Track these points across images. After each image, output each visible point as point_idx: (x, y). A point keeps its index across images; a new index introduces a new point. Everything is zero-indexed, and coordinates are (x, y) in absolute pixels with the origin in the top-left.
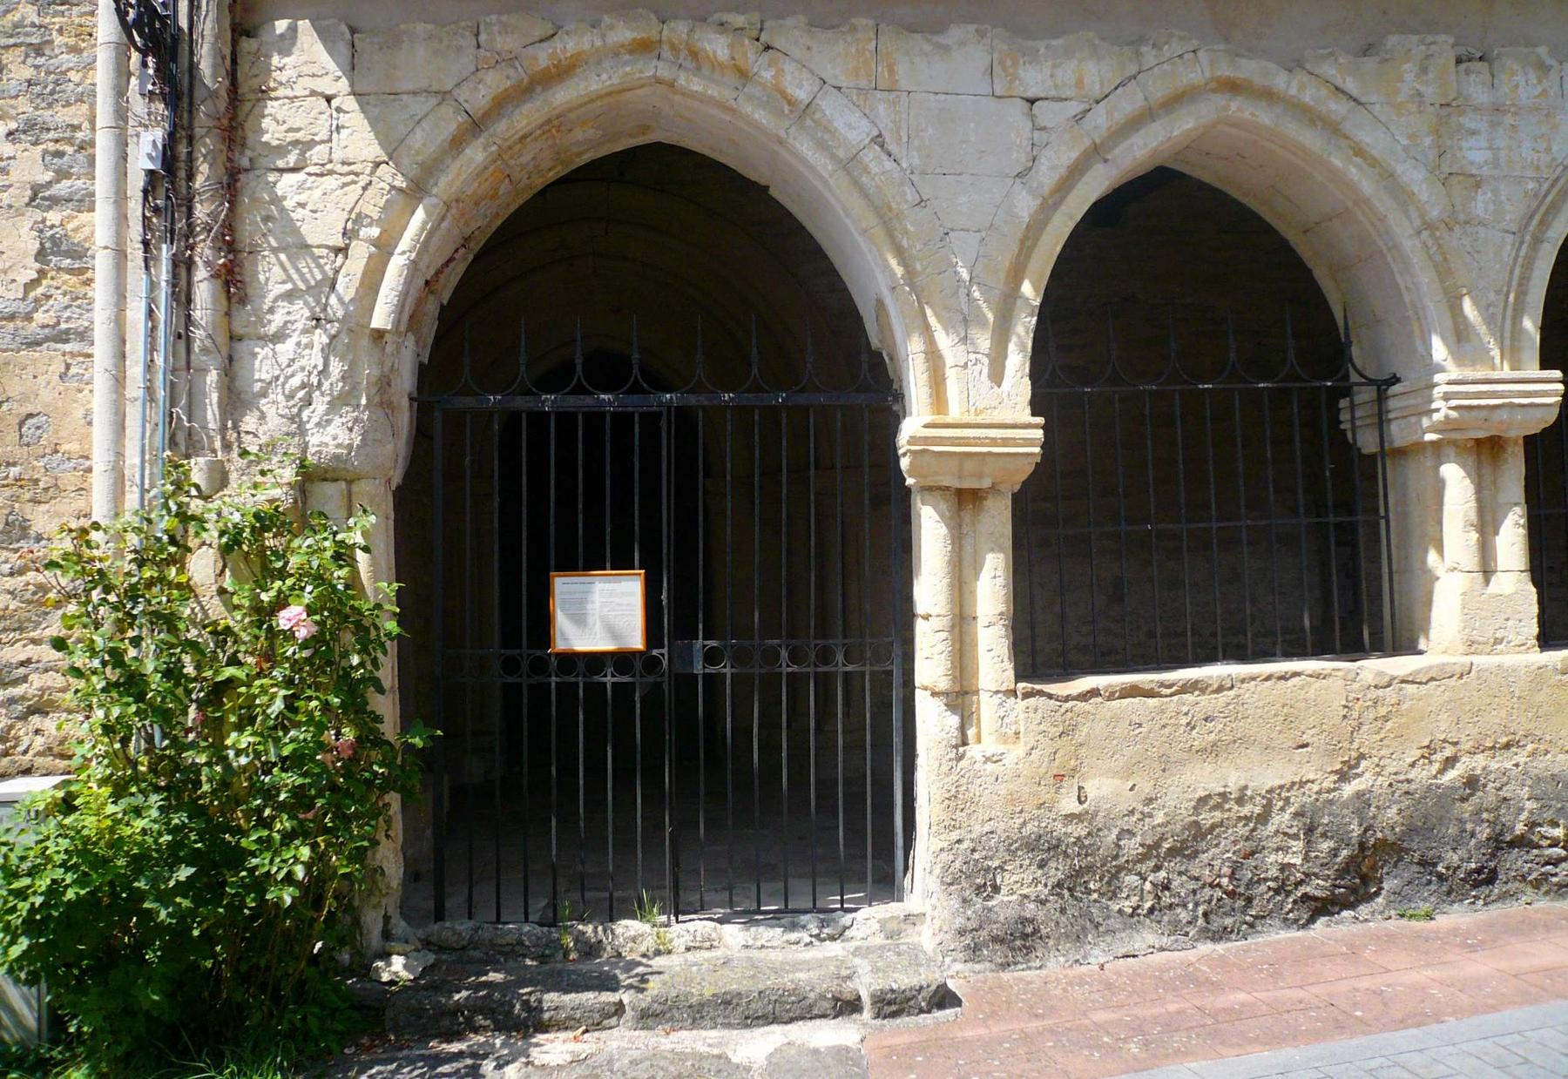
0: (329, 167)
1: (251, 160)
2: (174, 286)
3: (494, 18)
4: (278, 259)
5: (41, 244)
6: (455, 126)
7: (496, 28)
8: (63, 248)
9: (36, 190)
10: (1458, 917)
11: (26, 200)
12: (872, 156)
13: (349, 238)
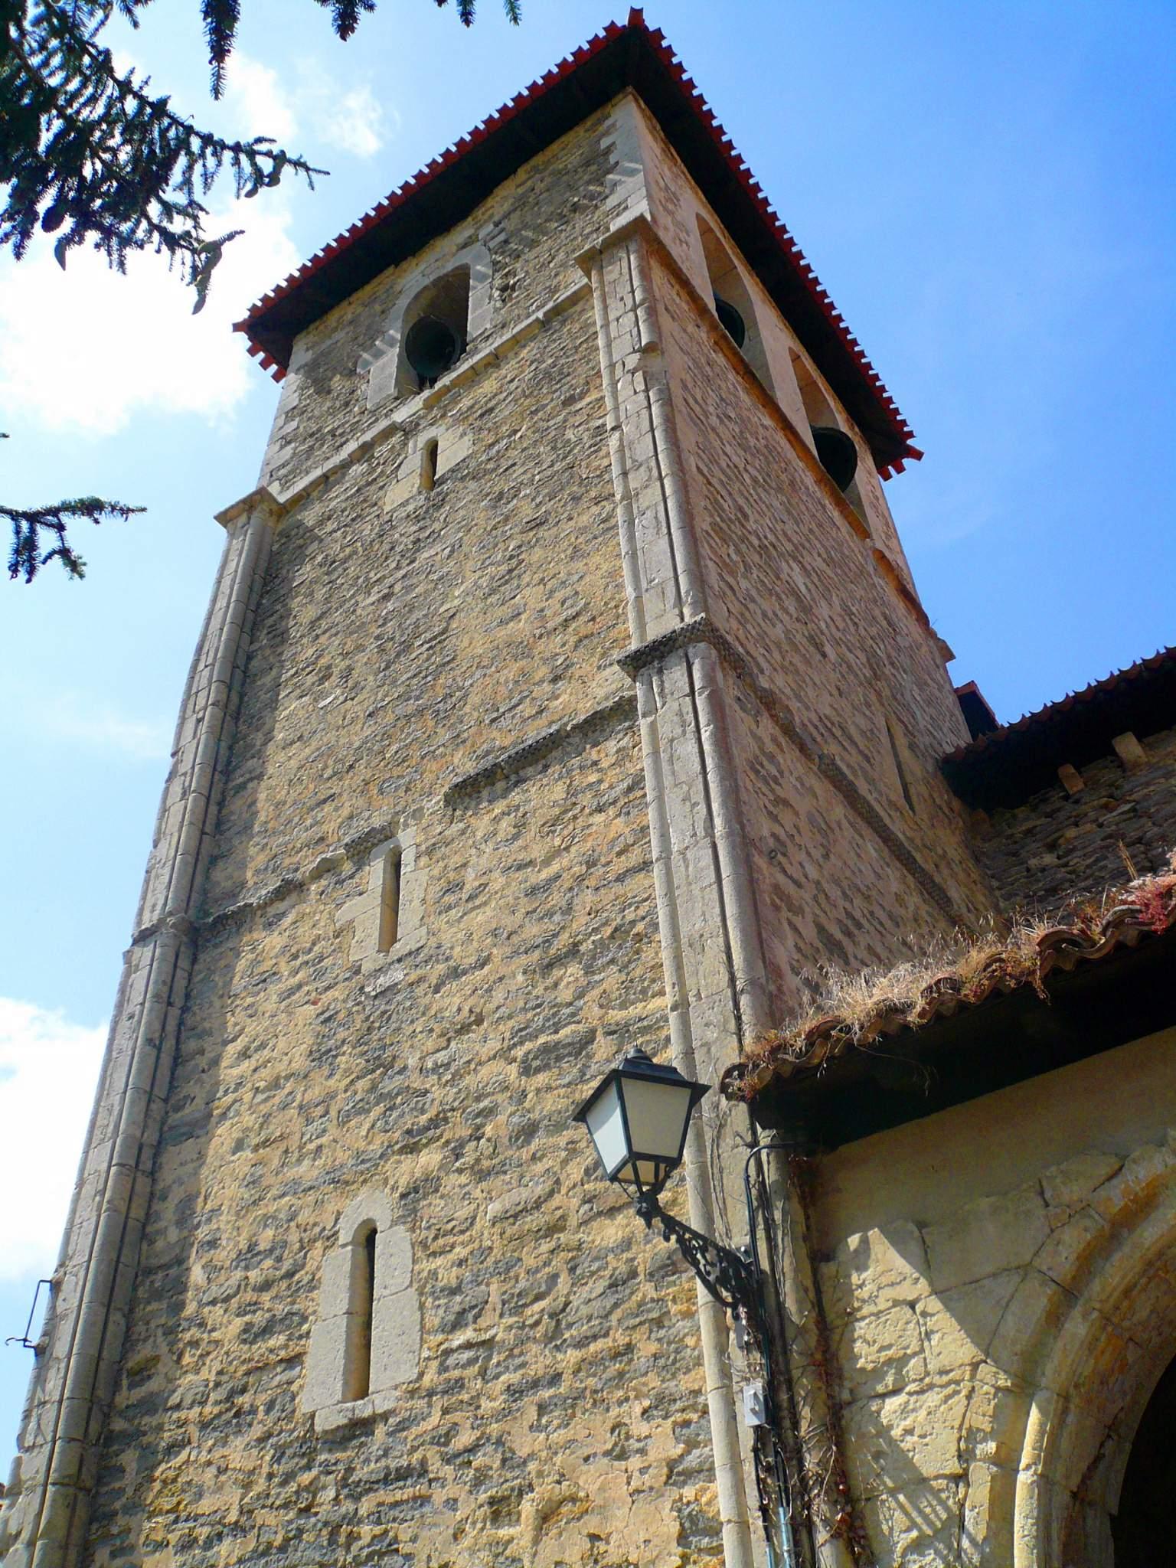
0: (927, 1380)
1: (851, 1391)
2: (797, 1555)
3: (1054, 1169)
4: (897, 1501)
5: (682, 1525)
6: (1045, 1301)
7: (1058, 1180)
8: (701, 1525)
9: (672, 1465)
11: (664, 1478)
13: (967, 1461)
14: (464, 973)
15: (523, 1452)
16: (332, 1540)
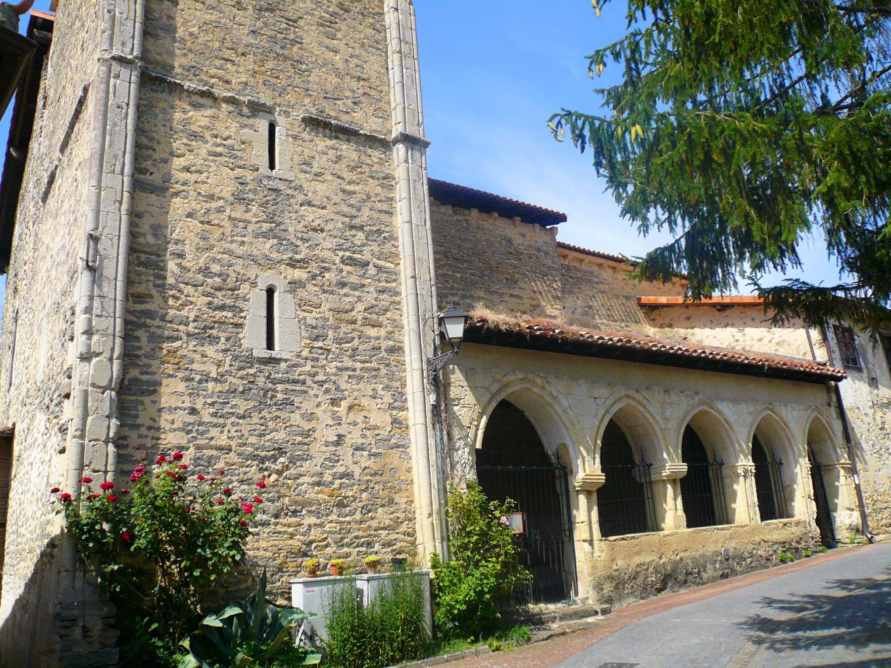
9: (390, 404)
10: (682, 591)
12: (569, 410)
14: (314, 206)
15: (343, 388)
16: (265, 395)
